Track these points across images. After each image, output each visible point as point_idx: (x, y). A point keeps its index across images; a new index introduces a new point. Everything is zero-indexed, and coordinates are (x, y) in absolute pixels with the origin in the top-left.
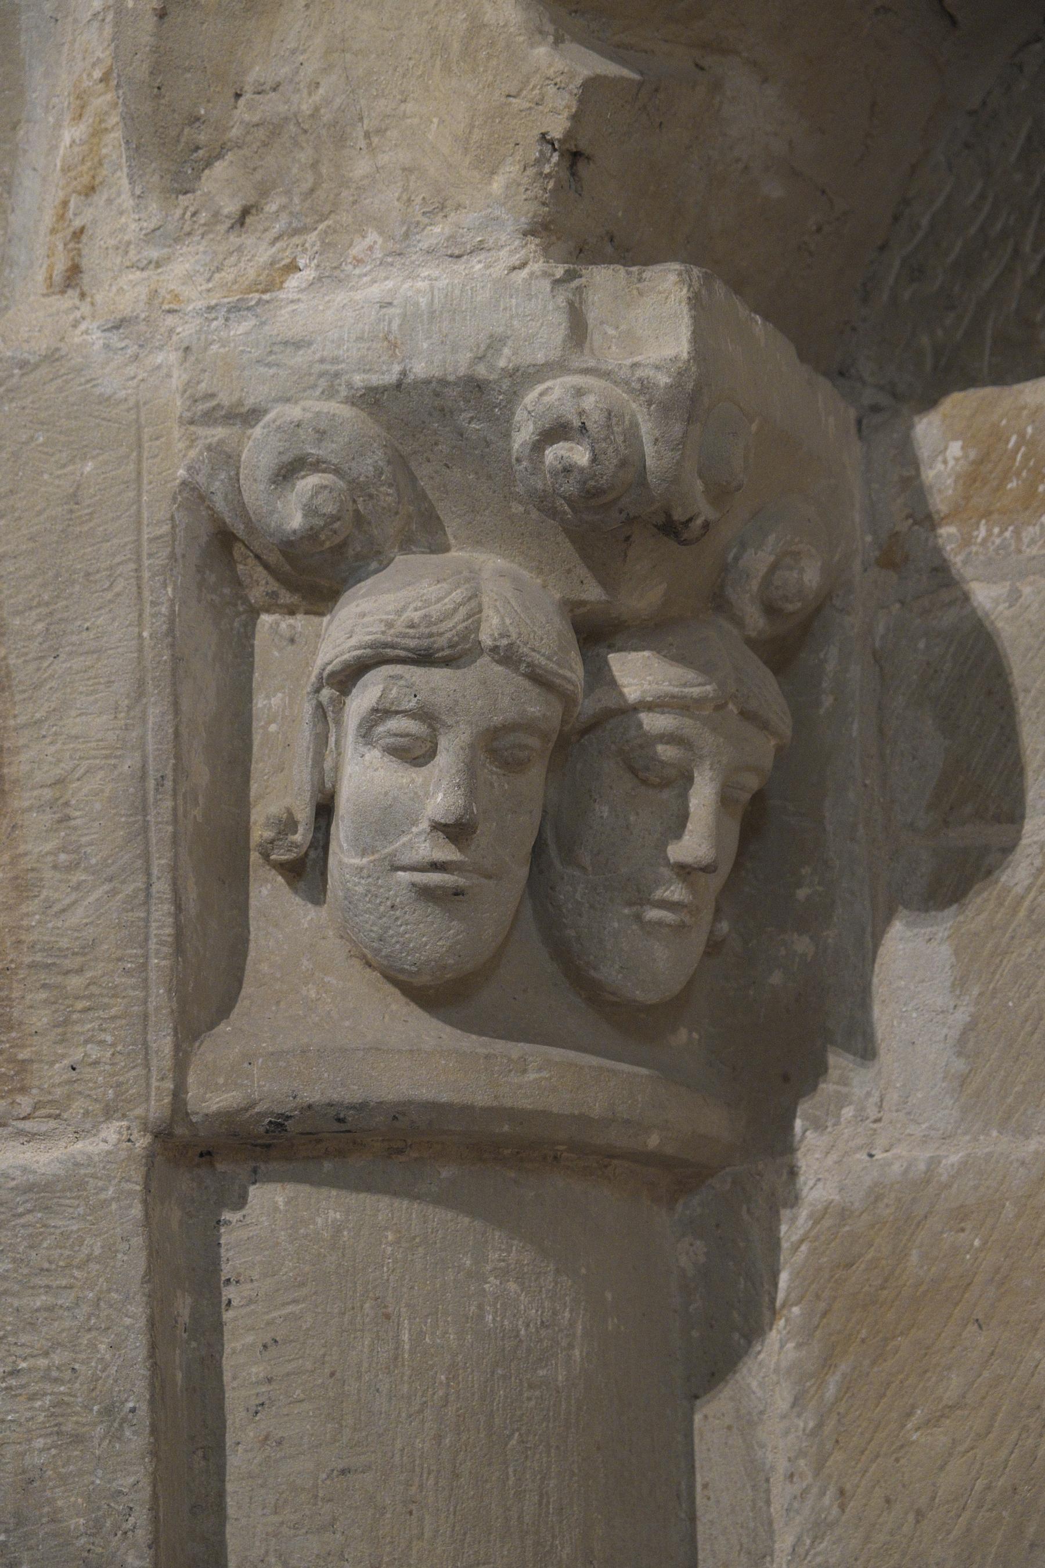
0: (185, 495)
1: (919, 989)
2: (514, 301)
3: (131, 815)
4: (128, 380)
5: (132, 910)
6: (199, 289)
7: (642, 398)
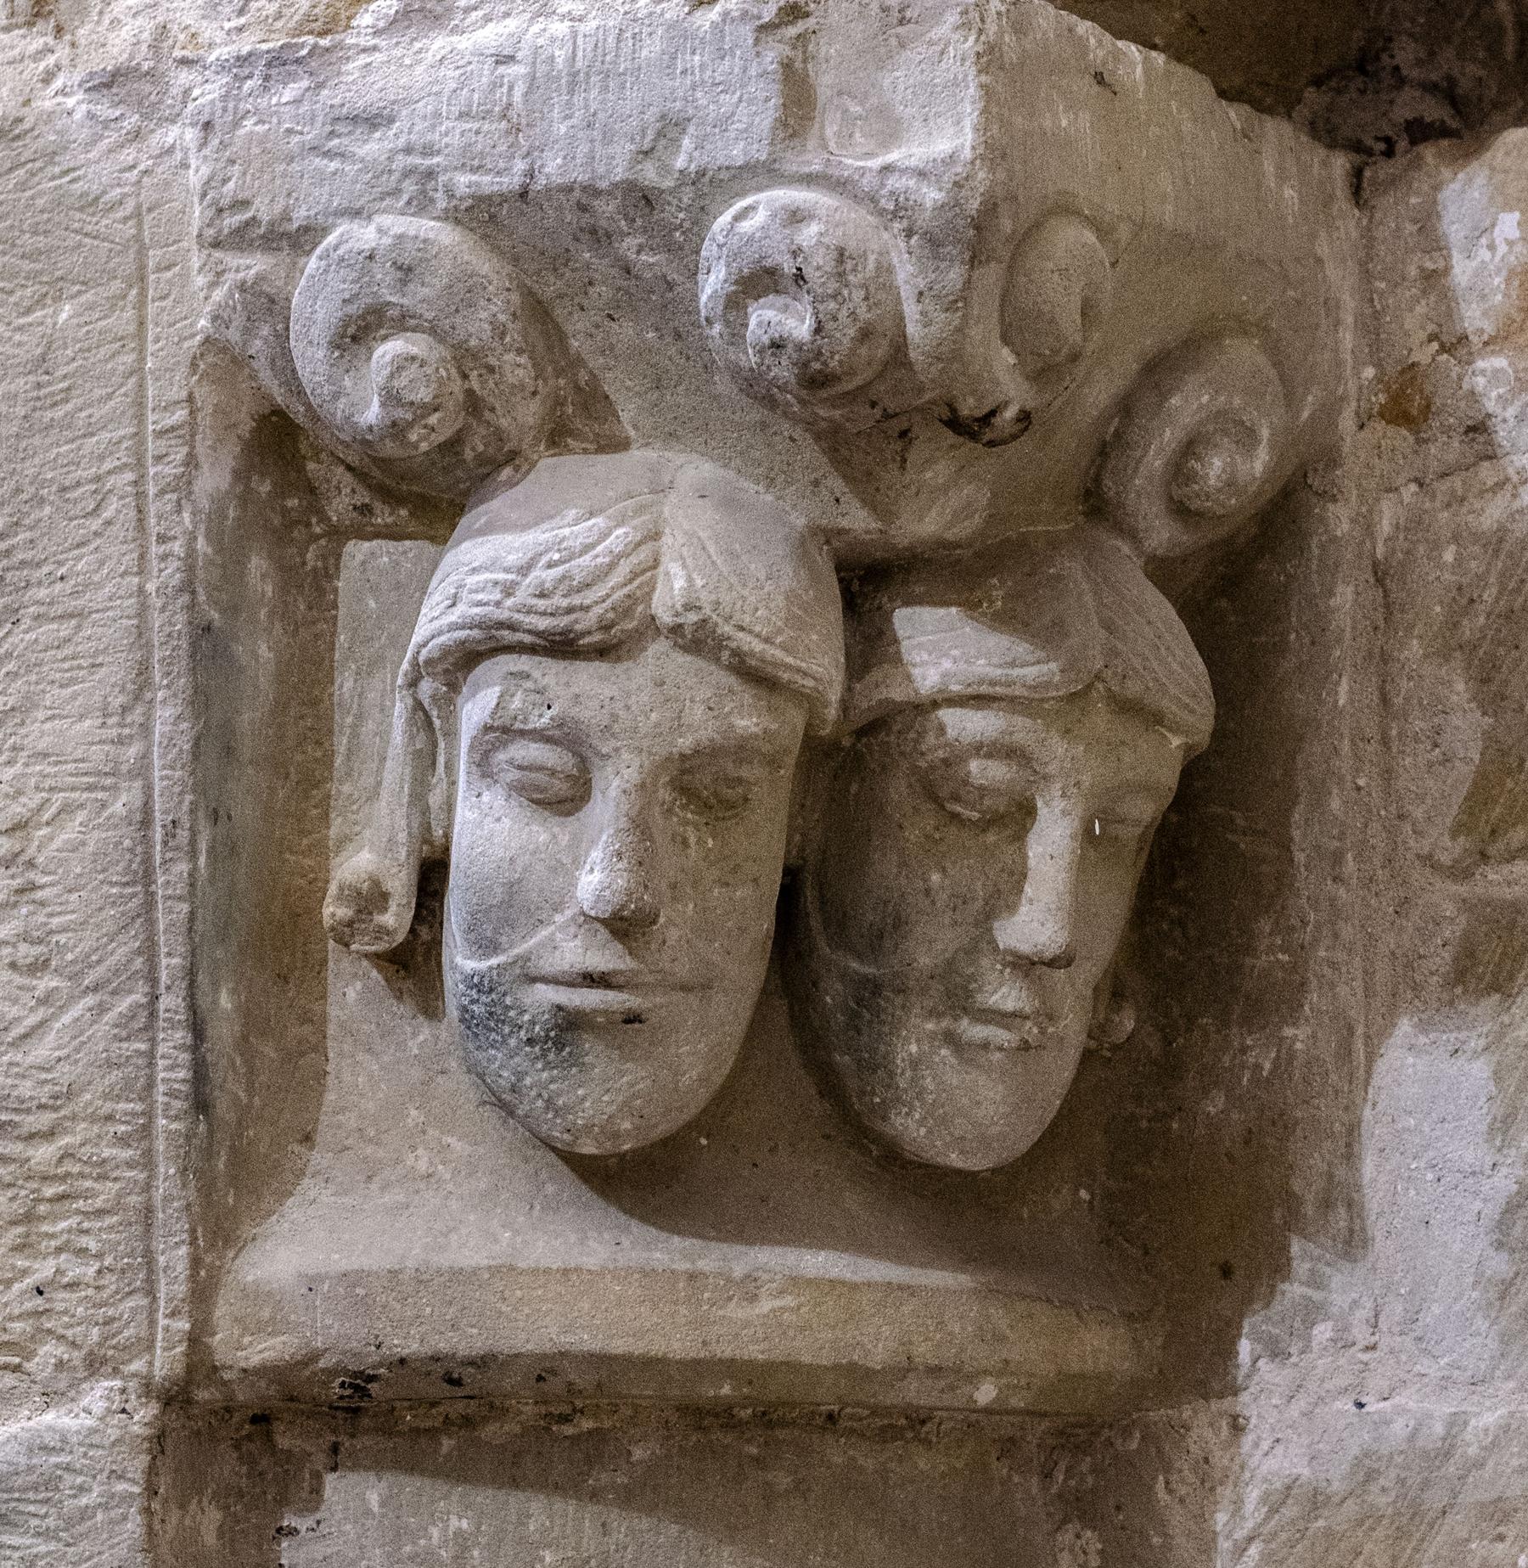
0: (210, 359)
1: (1438, 1133)
2: (697, 58)
3: (127, 884)
4: (122, 171)
5: (128, 1039)
6: (227, 25)
7: (897, 225)
